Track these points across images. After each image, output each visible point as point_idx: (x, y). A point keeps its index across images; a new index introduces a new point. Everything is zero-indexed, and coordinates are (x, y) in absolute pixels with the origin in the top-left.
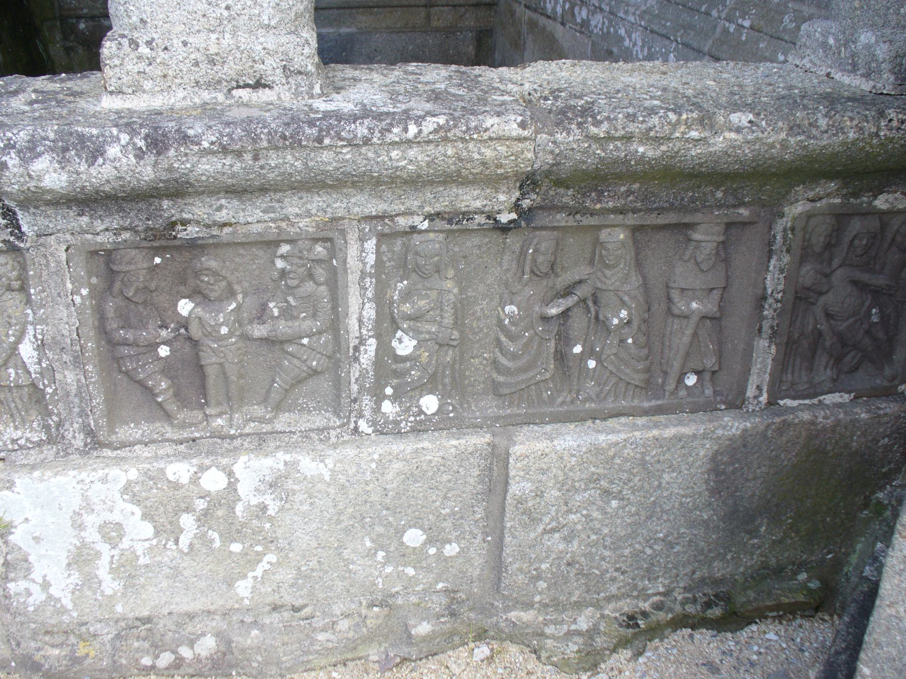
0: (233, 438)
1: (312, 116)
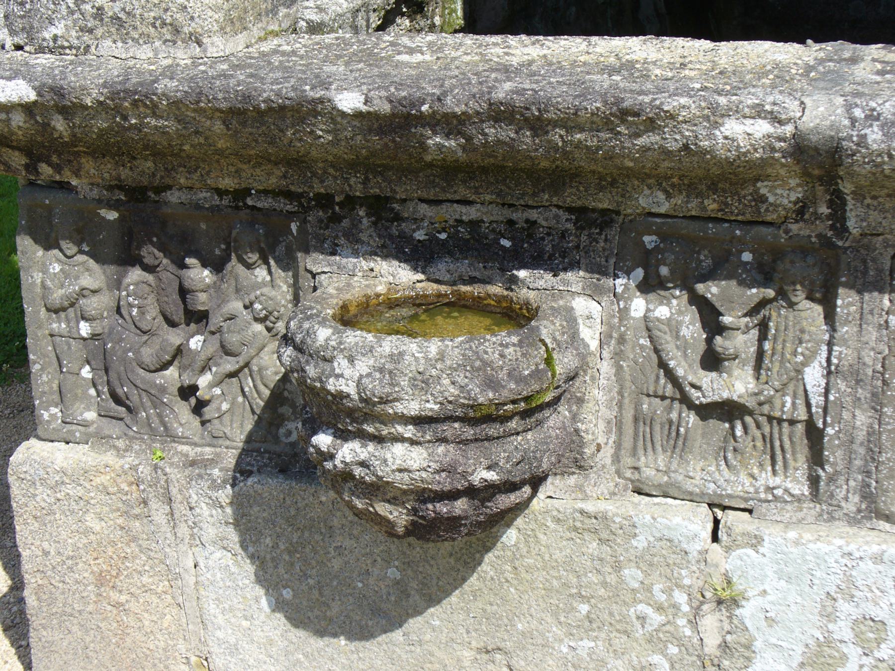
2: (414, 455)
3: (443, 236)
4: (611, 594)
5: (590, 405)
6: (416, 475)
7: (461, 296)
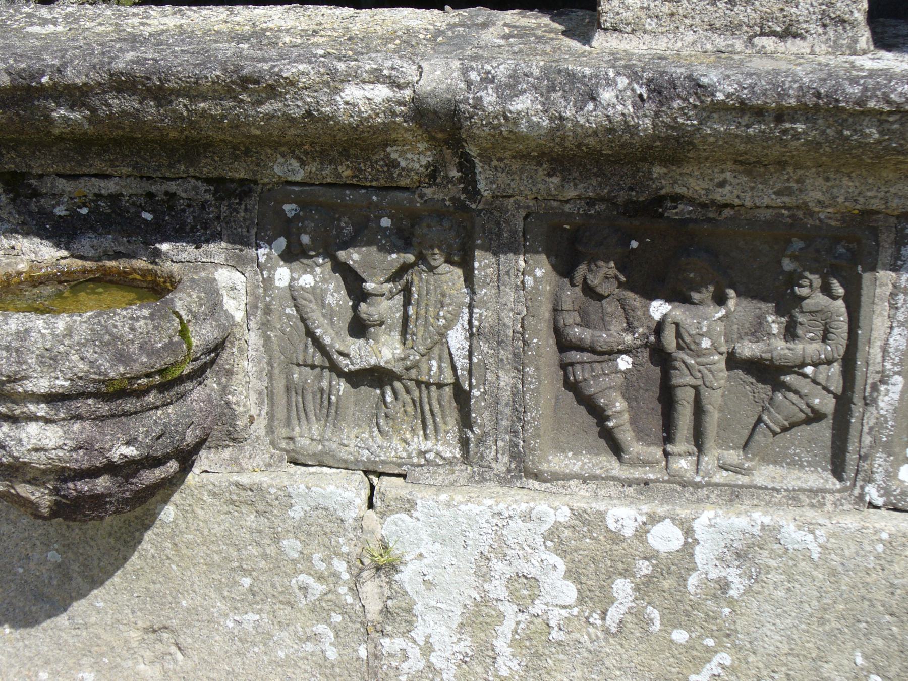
0: (697, 486)
1: (854, 73)
2: (49, 434)
3: (84, 211)
4: (271, 566)
5: (240, 377)
6: (53, 454)
7: (106, 272)
